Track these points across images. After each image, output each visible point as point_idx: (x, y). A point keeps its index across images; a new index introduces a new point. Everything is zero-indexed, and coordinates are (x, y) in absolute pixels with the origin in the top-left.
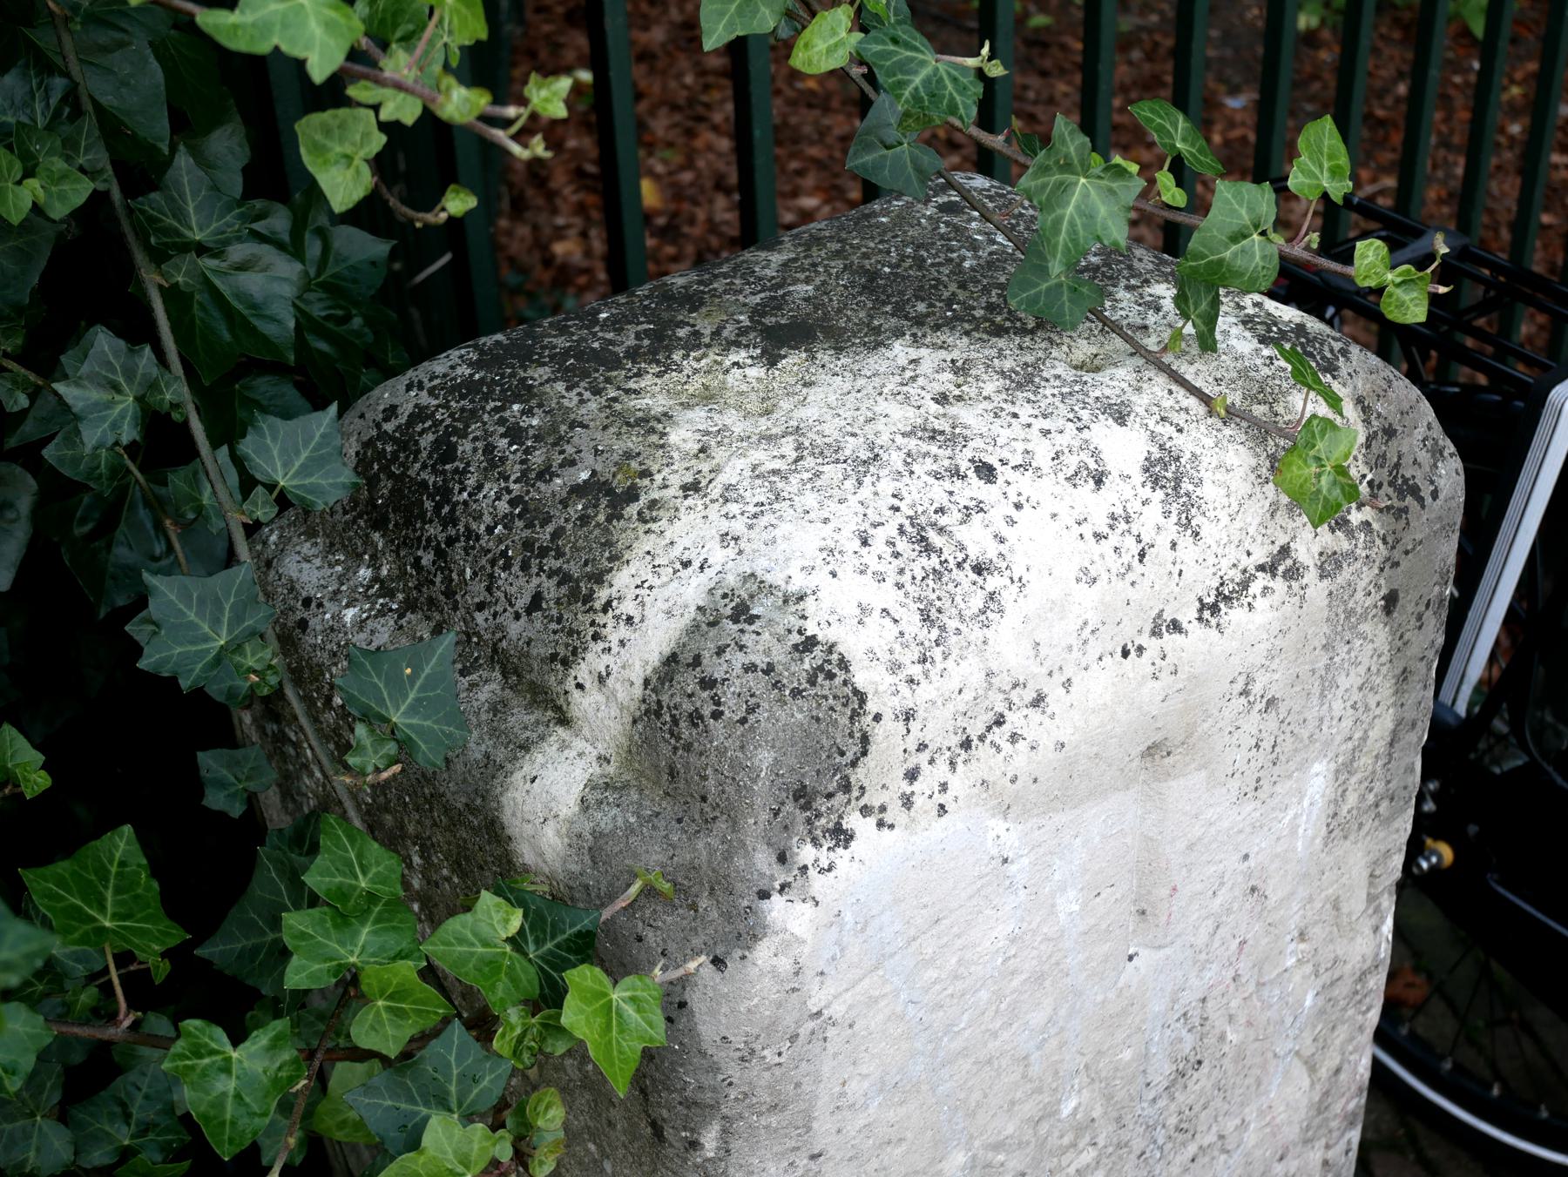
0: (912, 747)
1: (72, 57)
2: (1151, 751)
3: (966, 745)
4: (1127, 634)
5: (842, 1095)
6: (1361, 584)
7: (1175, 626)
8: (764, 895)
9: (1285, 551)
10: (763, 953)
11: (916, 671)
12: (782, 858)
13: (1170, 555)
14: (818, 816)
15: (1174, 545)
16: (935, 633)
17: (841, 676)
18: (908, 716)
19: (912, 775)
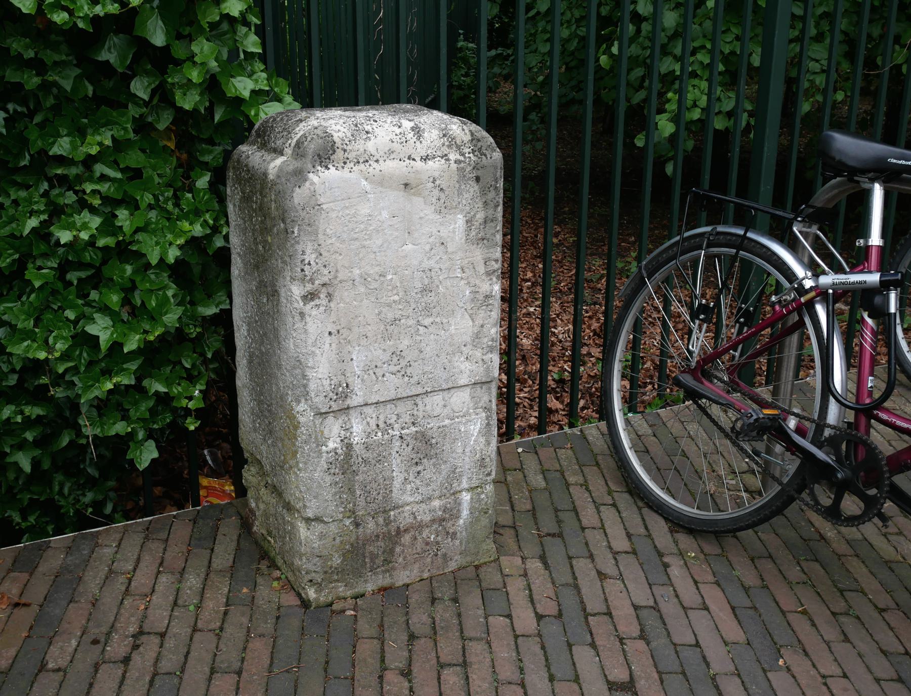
1: (649, 258)
2: (406, 185)
4: (402, 156)
6: (467, 170)
7: (414, 160)
8: (309, 172)
10: (307, 184)
11: (348, 143)
12: (314, 167)
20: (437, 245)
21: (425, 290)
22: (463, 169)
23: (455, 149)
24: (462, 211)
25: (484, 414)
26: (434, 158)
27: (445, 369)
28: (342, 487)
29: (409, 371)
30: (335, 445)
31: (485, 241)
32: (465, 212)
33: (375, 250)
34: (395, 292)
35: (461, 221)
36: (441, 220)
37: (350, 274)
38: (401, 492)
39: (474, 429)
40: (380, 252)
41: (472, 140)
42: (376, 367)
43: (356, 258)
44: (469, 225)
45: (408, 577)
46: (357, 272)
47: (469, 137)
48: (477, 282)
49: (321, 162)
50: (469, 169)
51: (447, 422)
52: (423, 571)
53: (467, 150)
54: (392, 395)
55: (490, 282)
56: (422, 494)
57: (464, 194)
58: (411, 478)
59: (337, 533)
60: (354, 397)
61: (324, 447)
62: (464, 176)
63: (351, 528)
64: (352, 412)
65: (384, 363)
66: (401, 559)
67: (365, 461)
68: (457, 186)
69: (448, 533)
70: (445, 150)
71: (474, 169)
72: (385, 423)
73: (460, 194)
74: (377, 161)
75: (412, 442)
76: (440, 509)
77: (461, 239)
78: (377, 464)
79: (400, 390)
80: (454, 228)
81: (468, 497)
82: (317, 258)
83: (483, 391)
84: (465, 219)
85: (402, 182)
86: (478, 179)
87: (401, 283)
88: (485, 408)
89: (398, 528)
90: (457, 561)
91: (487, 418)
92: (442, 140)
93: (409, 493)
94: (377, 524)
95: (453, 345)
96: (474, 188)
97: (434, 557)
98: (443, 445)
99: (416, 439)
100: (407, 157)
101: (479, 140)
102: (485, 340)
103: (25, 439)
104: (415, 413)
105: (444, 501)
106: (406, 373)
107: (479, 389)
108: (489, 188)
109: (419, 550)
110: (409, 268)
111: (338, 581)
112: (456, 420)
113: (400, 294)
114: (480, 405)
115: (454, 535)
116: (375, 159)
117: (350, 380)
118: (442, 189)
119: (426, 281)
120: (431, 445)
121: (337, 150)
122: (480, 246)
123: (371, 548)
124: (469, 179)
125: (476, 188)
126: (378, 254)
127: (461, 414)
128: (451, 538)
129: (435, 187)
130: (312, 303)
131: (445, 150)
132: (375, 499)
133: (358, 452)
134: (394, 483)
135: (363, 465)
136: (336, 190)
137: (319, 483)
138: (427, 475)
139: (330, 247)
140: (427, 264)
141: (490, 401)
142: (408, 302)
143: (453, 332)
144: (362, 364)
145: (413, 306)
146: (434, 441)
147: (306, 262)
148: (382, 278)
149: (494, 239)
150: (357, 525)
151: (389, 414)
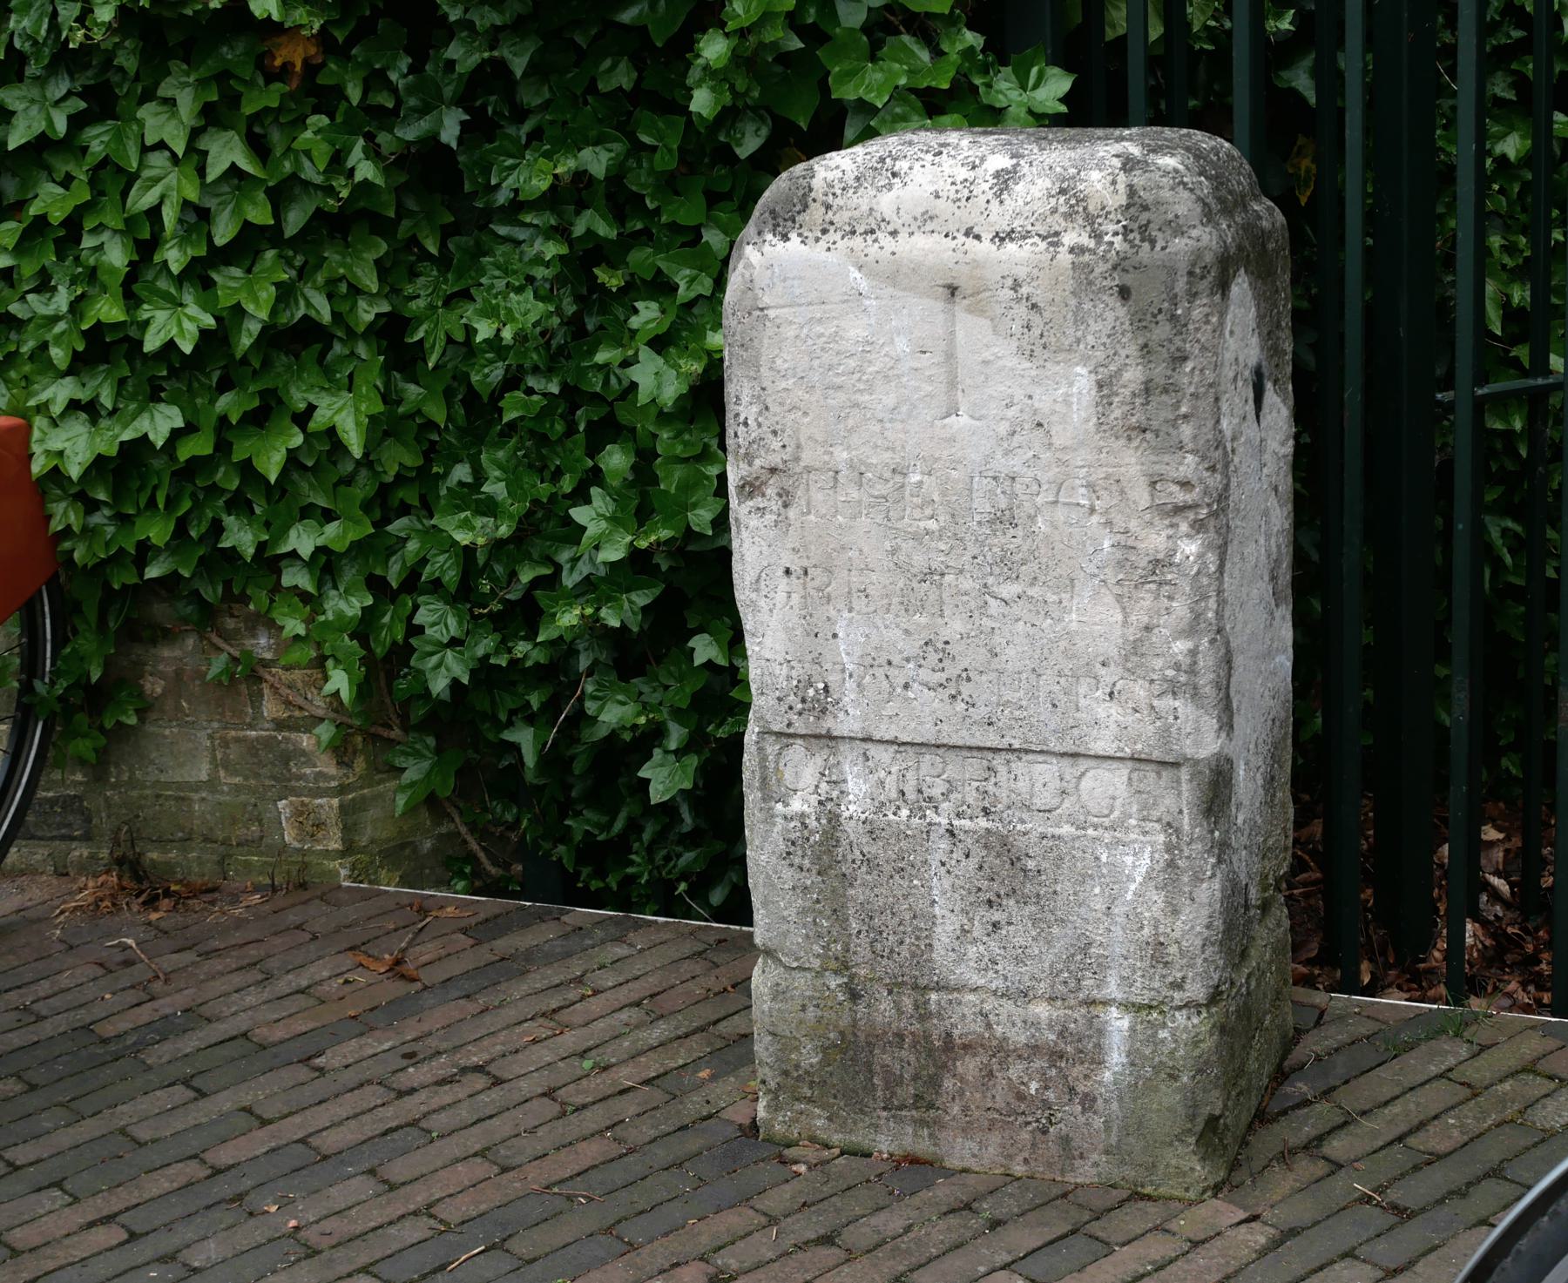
4: (951, 227)
7: (978, 237)
20: (1026, 426)
21: (1003, 519)
22: (1088, 269)
23: (1080, 221)
24: (1085, 360)
25: (1161, 838)
26: (1025, 238)
27: (1054, 706)
28: (818, 901)
29: (966, 689)
30: (805, 807)
31: (1149, 435)
32: (1093, 362)
33: (880, 416)
34: (928, 512)
35: (1084, 381)
36: (1034, 373)
37: (826, 458)
38: (953, 955)
39: (1134, 866)
40: (891, 420)
41: (1128, 206)
42: (890, 663)
43: (841, 426)
44: (1105, 392)
45: (974, 1156)
46: (841, 455)
47: (1122, 199)
48: (1133, 525)
49: (776, 226)
50: (1101, 268)
51: (1066, 830)
52: (1010, 1157)
53: (1112, 228)
54: (927, 733)
55: (1170, 532)
56: (1006, 978)
57: (1091, 322)
58: (978, 932)
59: (811, 998)
60: (841, 715)
61: (779, 806)
62: (1090, 283)
63: (841, 997)
64: (844, 747)
65: (908, 660)
66: (956, 1109)
67: (867, 860)
68: (1073, 302)
69: (1072, 1090)
70: (1057, 223)
71: (1115, 268)
72: (920, 791)
73: (1080, 319)
74: (894, 233)
75: (978, 853)
76: (1050, 1027)
77: (1088, 421)
78: (897, 877)
79: (945, 727)
80: (1067, 395)
81: (1125, 1023)
82: (760, 413)
83: (1162, 783)
84: (1093, 376)
85: (941, 282)
86: (1124, 293)
87: (943, 494)
88: (1169, 824)
89: (949, 1035)
90: (1096, 1164)
91: (1169, 848)
92: (1053, 201)
93: (972, 964)
94: (900, 1012)
95: (1074, 656)
96: (1114, 313)
97: (1039, 1135)
98: (1056, 882)
99: (986, 846)
100: (963, 231)
101: (1145, 208)
102: (1158, 663)
103: (528, 703)
104: (991, 788)
105: (1061, 1012)
106: (960, 693)
107: (1153, 775)
108: (1154, 316)
109: (1000, 1103)
110: (959, 467)
111: (810, 1100)
112: (1090, 832)
113: (941, 518)
114: (1155, 814)
115: (1088, 1102)
116: (890, 228)
117: (833, 679)
118: (1034, 306)
119: (1003, 503)
120: (1024, 871)
121: (813, 206)
122: (1135, 443)
123: (887, 1059)
124: (1102, 290)
125: (1122, 311)
126: (888, 425)
127: (1106, 821)
128: (1082, 1103)
129: (1018, 300)
130: (750, 503)
131: (1057, 223)
132: (892, 951)
133: (852, 837)
134: (938, 930)
135: (864, 869)
136: (796, 283)
137: (768, 877)
138: (1019, 935)
139: (784, 394)
140: (1001, 464)
141: (1181, 812)
142: (961, 540)
143: (1074, 626)
144: (858, 651)
145: (973, 549)
146: (1031, 864)
147: (742, 419)
148: (898, 478)
149: (1173, 432)
150: (854, 996)
151: (930, 773)
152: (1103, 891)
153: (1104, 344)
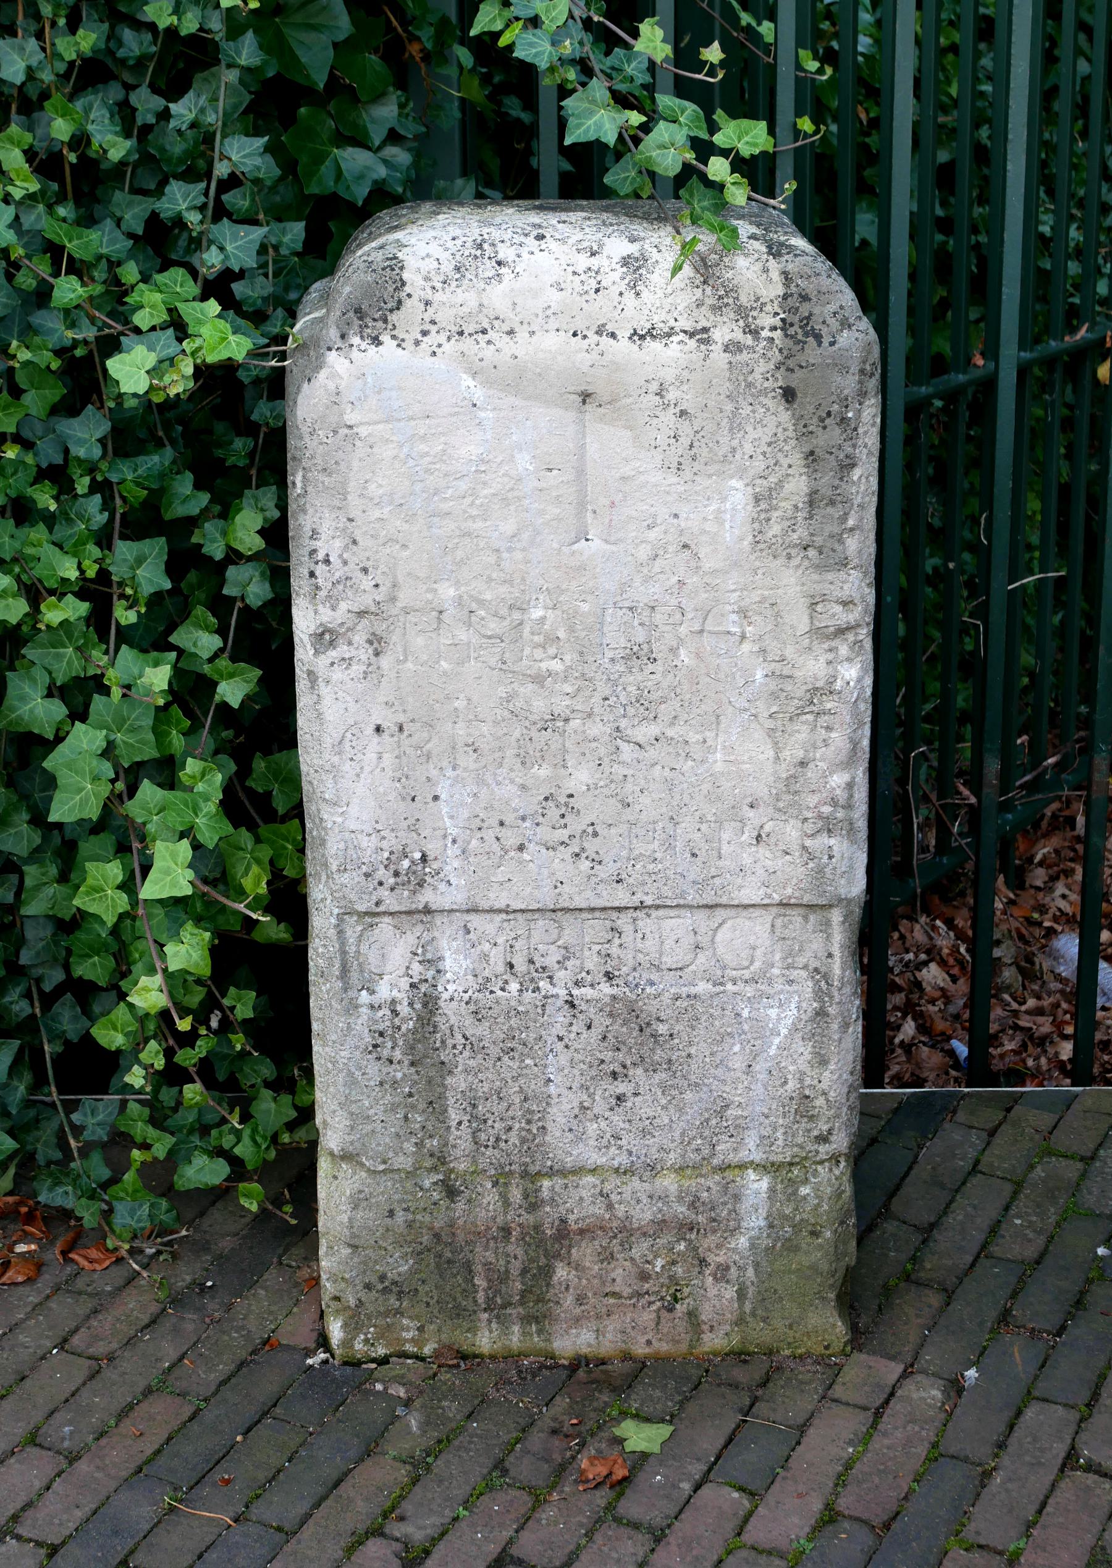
0: (428, 320)
3: (461, 333)
5: (365, 488)
7: (613, 335)
8: (329, 349)
9: (705, 330)
11: (439, 285)
13: (618, 298)
14: (367, 326)
15: (621, 294)
16: (458, 276)
17: (397, 271)
18: (427, 303)
19: (425, 333)
57: (749, 429)
152: (743, 1049)
153: (764, 454)
